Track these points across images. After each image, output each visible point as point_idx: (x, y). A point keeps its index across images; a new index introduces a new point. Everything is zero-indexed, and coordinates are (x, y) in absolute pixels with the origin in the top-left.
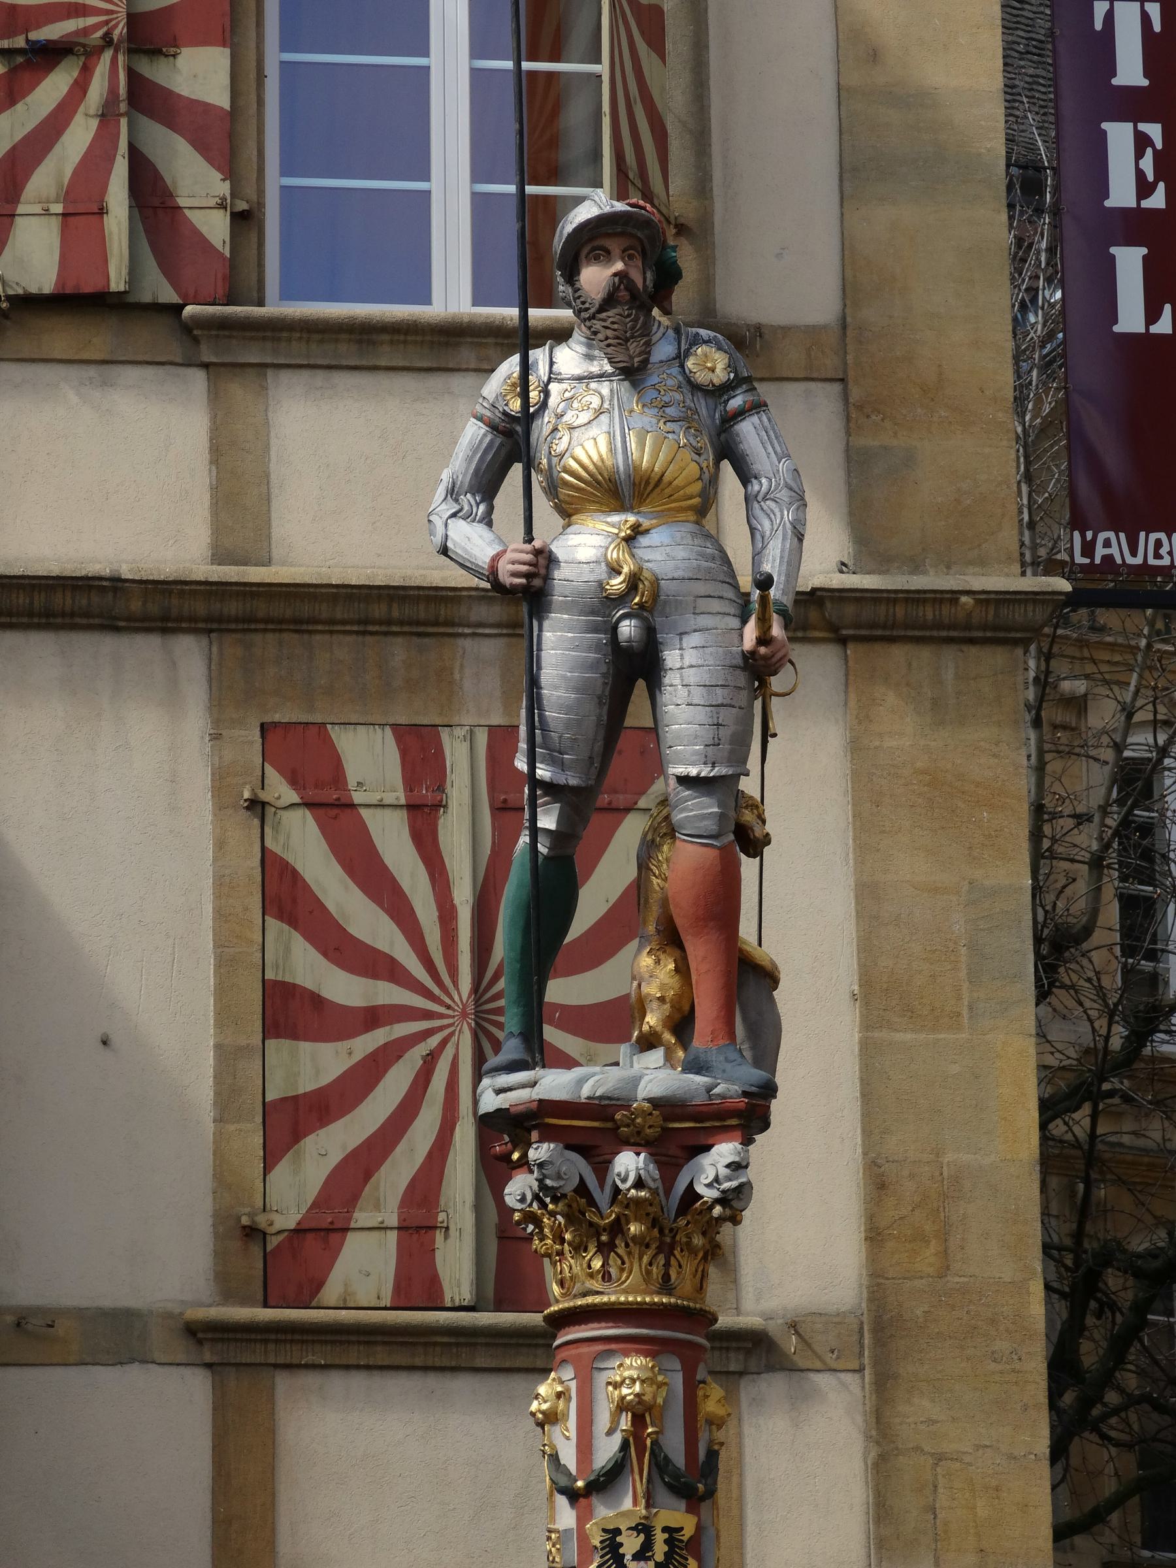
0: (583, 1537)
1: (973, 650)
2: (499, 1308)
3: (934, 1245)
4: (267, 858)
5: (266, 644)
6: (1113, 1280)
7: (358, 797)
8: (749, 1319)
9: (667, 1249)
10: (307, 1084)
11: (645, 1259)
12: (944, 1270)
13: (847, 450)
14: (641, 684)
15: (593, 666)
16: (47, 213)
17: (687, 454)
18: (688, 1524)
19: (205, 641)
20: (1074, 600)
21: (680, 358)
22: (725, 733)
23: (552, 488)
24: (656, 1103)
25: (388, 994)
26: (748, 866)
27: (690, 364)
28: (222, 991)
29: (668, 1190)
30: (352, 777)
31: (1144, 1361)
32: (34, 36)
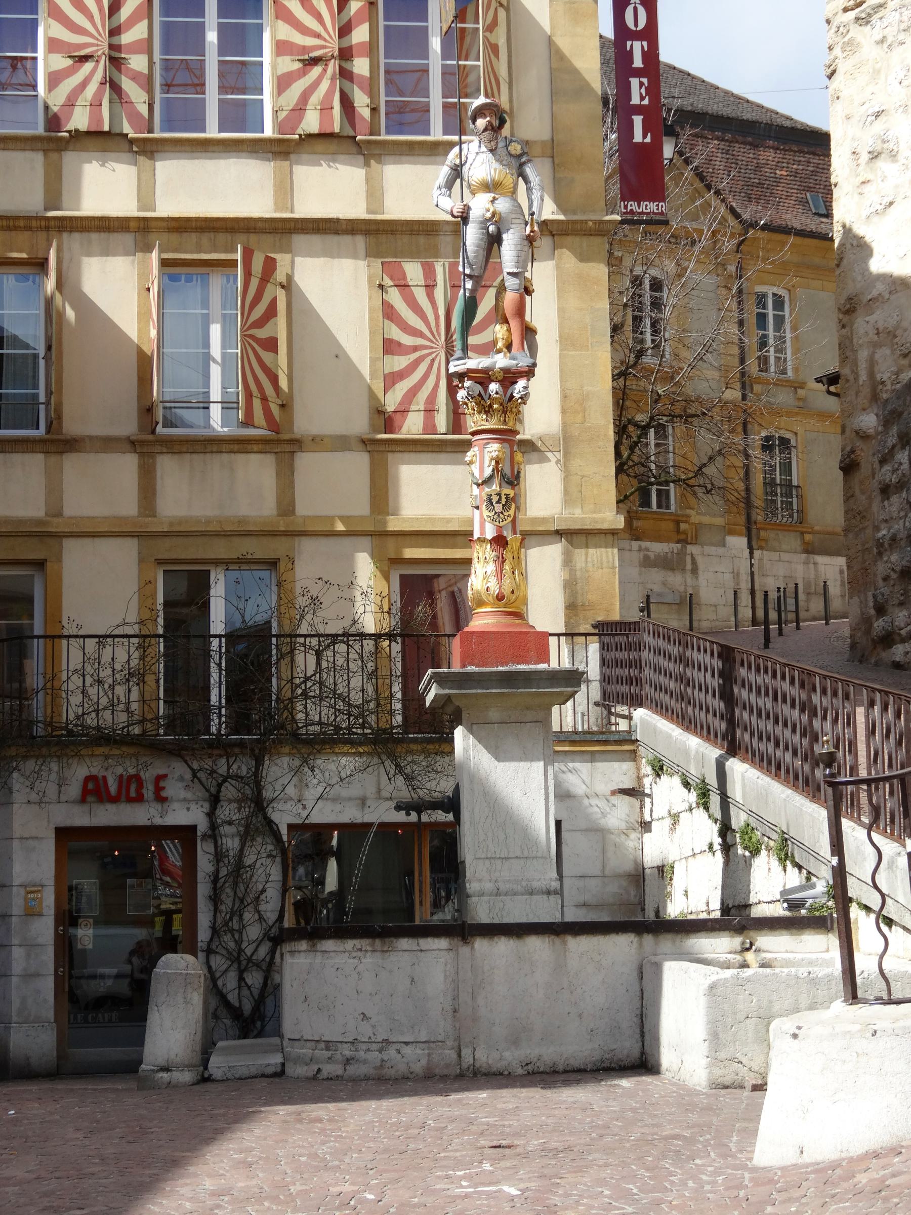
0: (481, 497)
1: (592, 238)
2: (453, 433)
4: (384, 302)
5: (383, 238)
6: (631, 428)
7: (410, 283)
8: (526, 436)
9: (505, 412)
10: (396, 369)
12: (584, 422)
14: (496, 245)
15: (482, 240)
17: (509, 176)
18: (512, 493)
20: (622, 222)
21: (507, 146)
22: (521, 259)
23: (469, 186)
24: (501, 369)
25: (420, 341)
26: (528, 298)
28: (372, 341)
29: (505, 395)
30: (409, 277)
31: (639, 452)
32: (311, 55)
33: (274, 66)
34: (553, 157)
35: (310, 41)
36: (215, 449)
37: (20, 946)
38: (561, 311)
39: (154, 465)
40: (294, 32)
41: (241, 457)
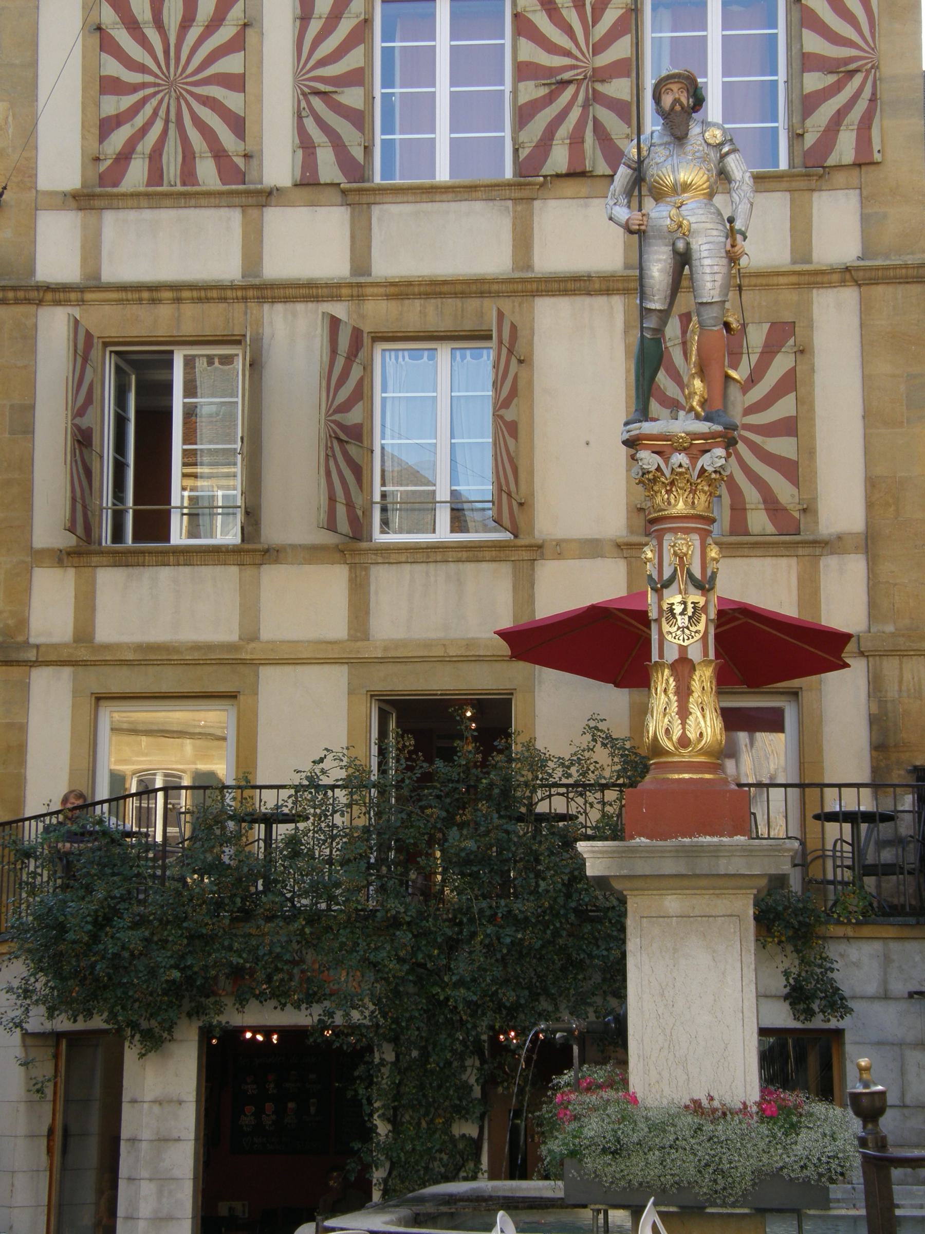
3: (892, 509)
11: (685, 496)
13: (861, 215)
16: (563, 144)
19: (622, 297)
21: (703, 133)
27: (707, 135)
33: (515, 92)
34: (860, 188)
35: (558, 61)
36: (439, 558)
37: (150, 1180)
38: (867, 379)
39: (367, 577)
40: (540, 51)
41: (470, 567)
